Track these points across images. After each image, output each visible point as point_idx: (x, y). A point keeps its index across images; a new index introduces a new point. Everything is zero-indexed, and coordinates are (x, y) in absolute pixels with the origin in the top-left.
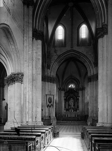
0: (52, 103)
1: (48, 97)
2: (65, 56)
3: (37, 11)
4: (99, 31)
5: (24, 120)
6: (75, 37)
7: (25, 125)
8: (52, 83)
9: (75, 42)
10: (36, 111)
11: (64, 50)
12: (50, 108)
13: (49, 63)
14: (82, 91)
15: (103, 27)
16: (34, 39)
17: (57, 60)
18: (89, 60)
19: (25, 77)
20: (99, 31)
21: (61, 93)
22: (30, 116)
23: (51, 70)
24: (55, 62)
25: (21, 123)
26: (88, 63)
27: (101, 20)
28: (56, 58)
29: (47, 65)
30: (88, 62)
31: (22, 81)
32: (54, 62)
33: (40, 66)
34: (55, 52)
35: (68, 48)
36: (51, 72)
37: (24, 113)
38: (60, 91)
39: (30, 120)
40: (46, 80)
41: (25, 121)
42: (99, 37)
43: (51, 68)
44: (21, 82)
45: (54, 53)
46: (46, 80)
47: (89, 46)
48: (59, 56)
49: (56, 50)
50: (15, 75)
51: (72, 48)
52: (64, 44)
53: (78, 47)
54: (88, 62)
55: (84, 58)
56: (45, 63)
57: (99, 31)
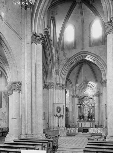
0: (61, 113)
1: (56, 106)
2: (75, 60)
3: (36, 12)
4: (106, 26)
5: (22, 133)
6: (86, 37)
7: (23, 138)
8: (61, 90)
9: (86, 42)
10: (37, 123)
11: (74, 52)
12: (60, 119)
13: (58, 68)
14: (98, 97)
15: (111, 21)
16: (33, 44)
17: (67, 64)
18: (103, 61)
19: (23, 86)
20: (107, 26)
21: (74, 100)
22: (29, 128)
23: (60, 76)
24: (65, 67)
25: (19, 136)
26: (103, 65)
27: (40, 13)
28: (65, 62)
29: (56, 70)
30: (101, 63)
31: (20, 90)
32: (63, 67)
33: (40, 73)
34: (64, 55)
35: (79, 50)
36: (60, 78)
37: (22, 125)
38: (73, 98)
39: (30, 132)
40: (55, 87)
41: (24, 134)
42: (107, 33)
43: (59, 74)
44: (18, 91)
45: (63, 56)
46: (55, 87)
47: (103, 45)
48: (69, 60)
49: (66, 53)
50: (12, 84)
51: (83, 49)
52: (74, 45)
53: (90, 47)
54: (101, 63)
55: (97, 59)
56: (53, 69)
57: (107, 26)
